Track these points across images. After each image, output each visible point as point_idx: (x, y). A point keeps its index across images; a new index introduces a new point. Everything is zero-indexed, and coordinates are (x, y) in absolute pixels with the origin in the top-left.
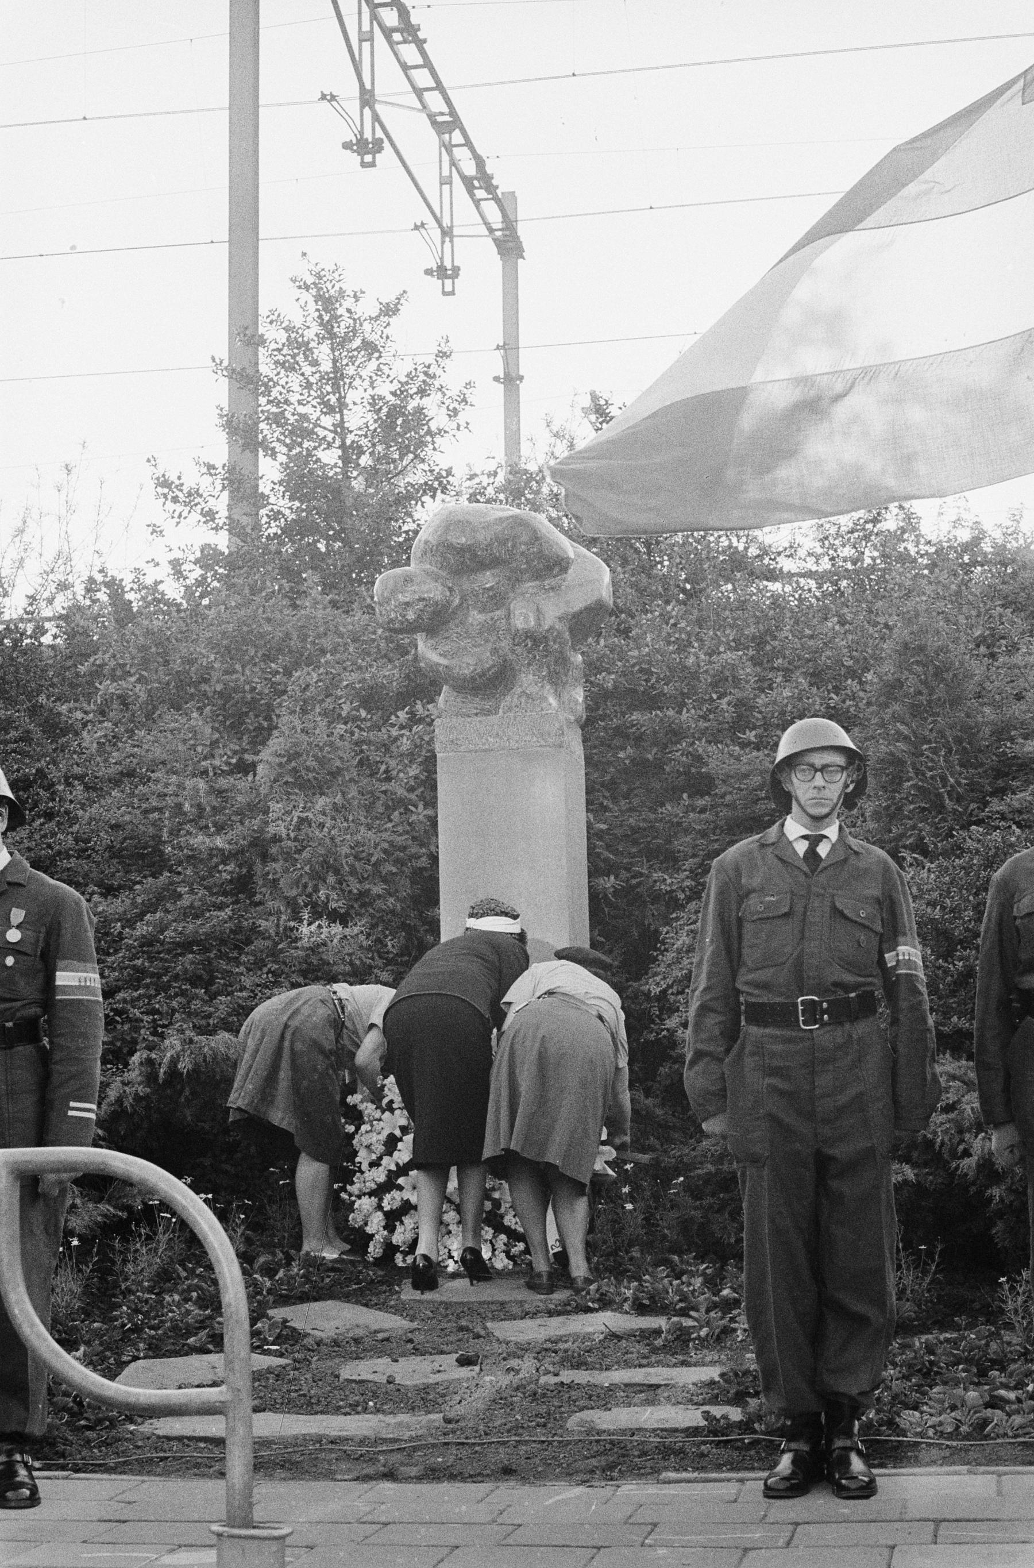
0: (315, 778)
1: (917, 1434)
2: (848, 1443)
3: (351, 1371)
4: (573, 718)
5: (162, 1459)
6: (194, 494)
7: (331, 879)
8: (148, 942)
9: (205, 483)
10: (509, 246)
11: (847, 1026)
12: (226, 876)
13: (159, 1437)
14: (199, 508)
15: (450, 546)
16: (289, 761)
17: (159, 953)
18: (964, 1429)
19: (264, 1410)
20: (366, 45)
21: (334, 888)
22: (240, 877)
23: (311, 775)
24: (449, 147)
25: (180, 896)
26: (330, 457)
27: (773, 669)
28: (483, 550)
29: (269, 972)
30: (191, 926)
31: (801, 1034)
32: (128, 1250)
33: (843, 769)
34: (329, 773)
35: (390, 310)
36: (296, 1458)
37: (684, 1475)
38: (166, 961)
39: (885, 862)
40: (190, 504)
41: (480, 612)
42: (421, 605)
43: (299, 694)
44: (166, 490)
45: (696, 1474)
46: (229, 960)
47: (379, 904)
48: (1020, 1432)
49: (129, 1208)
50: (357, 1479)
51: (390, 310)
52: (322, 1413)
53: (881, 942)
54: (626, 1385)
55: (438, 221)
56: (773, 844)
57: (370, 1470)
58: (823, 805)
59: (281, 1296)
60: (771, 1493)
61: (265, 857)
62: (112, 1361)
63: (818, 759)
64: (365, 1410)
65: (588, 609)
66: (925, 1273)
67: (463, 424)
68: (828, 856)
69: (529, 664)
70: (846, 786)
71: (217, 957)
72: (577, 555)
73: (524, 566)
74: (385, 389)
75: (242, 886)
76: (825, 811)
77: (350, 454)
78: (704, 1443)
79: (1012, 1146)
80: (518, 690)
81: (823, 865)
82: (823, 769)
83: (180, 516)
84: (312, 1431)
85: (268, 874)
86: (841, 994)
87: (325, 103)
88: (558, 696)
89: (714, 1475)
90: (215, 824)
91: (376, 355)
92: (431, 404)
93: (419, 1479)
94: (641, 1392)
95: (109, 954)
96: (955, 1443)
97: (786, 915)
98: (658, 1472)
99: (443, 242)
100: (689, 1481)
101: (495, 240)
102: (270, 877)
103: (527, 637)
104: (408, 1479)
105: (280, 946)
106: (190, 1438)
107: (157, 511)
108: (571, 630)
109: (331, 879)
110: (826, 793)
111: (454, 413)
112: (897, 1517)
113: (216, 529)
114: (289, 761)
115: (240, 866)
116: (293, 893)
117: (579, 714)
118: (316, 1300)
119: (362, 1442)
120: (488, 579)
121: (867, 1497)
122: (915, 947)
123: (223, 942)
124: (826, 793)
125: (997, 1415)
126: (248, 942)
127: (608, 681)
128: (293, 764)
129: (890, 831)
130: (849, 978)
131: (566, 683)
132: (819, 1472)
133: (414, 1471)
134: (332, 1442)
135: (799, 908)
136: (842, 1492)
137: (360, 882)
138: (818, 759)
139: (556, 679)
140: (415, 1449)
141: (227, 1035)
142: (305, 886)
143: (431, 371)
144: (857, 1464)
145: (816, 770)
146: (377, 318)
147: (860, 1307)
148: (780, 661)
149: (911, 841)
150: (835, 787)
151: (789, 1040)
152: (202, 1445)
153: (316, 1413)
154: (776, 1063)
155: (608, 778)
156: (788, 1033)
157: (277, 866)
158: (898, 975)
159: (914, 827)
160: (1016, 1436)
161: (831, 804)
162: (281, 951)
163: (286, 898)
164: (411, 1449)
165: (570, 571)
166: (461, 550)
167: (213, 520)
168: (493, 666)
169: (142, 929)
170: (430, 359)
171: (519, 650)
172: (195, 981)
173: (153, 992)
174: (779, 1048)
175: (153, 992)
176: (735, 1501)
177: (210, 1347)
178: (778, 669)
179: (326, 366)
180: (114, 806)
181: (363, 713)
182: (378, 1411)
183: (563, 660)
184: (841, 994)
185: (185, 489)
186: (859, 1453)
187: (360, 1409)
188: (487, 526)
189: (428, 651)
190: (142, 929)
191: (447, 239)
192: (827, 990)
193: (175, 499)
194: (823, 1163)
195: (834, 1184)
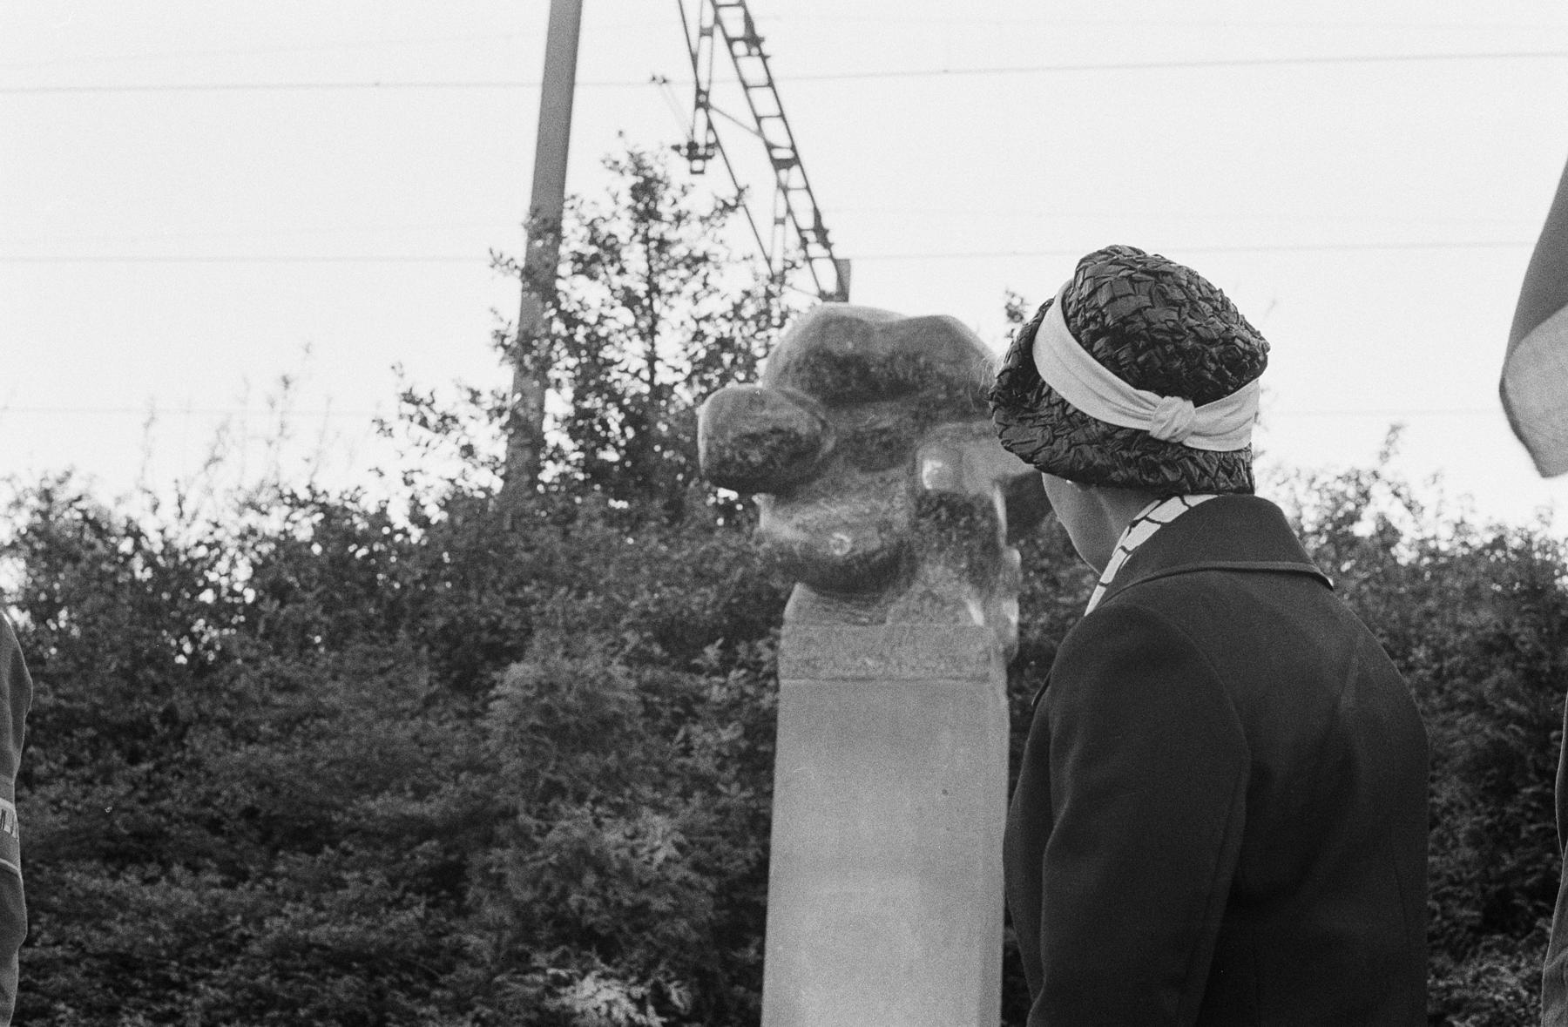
6: (446, 422)
7: (590, 879)
8: (283, 949)
9: (463, 410)
12: (421, 861)
15: (827, 356)
16: (540, 695)
17: (297, 969)
20: (706, 40)
21: (592, 894)
24: (785, 189)
25: (343, 885)
28: (879, 365)
41: (863, 470)
42: (774, 441)
46: (415, 994)
47: (663, 927)
61: (488, 841)
69: (940, 549)
71: (392, 985)
73: (942, 397)
75: (446, 883)
80: (918, 588)
85: (490, 865)
87: (654, 86)
90: (415, 788)
95: (217, 966)
102: (493, 870)
103: (941, 503)
105: (498, 979)
109: (590, 879)
114: (540, 695)
116: (527, 896)
120: (883, 417)
123: (407, 966)
128: (545, 700)
137: (635, 891)
139: (982, 575)
142: (548, 888)
149: (1530, 881)
157: (508, 855)
159: (1538, 859)
162: (499, 986)
163: (516, 904)
166: (843, 364)
171: (926, 523)
181: (657, 650)
185: (438, 408)
193: (424, 422)
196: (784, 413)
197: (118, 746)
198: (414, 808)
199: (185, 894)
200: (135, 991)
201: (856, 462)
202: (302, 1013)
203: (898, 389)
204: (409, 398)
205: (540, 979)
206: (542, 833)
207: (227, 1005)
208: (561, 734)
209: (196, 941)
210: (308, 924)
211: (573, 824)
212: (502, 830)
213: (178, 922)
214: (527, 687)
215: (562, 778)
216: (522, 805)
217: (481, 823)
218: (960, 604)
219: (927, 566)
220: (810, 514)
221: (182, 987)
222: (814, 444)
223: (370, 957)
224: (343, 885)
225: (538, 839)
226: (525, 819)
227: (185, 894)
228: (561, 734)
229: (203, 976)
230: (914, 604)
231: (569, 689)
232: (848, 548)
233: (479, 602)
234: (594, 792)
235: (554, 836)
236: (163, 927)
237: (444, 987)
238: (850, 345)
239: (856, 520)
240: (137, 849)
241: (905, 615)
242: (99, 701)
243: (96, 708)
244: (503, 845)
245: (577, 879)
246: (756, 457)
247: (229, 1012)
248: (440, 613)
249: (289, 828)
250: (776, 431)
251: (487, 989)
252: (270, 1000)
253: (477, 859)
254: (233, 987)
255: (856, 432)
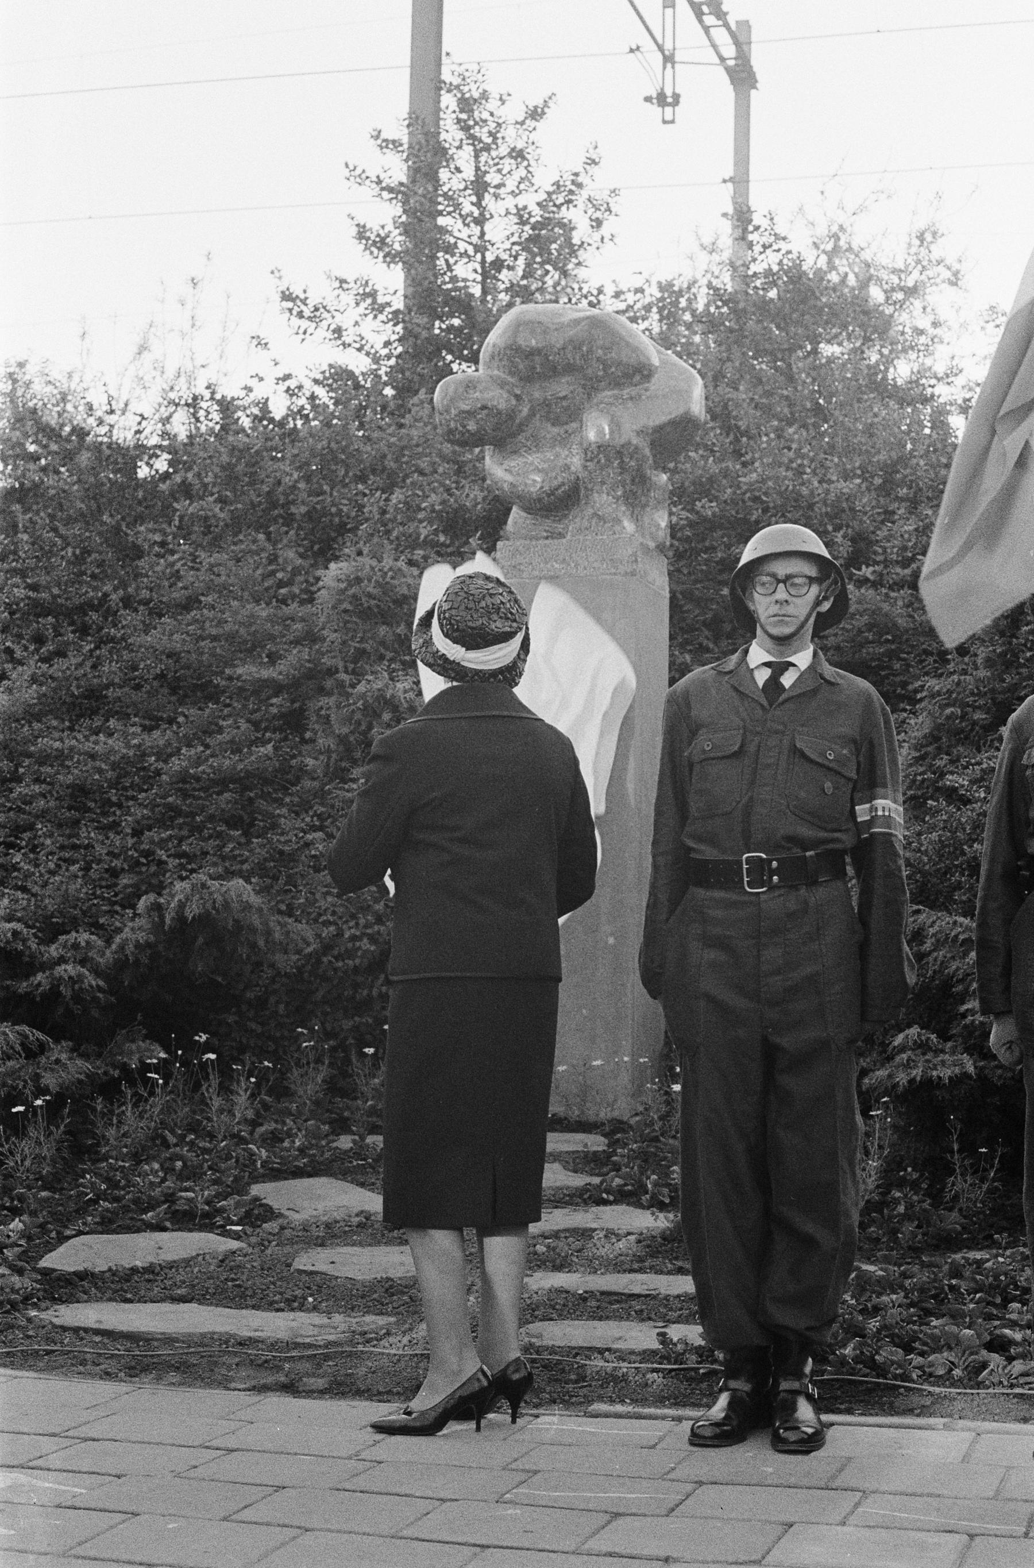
0: (378, 606)
1: (896, 1377)
2: (796, 1385)
3: (314, 1260)
4: (652, 545)
5: (48, 1353)
8: (184, 777)
10: (742, 76)
11: (803, 891)
12: (274, 710)
13: (55, 1326)
14: (325, 324)
18: (957, 1372)
19: (190, 1302)
22: (292, 713)
23: (373, 602)
26: (466, 271)
27: (896, 498)
29: (315, 814)
30: (227, 762)
31: (746, 898)
32: (111, 1112)
33: (811, 580)
34: (395, 602)
35: (536, 114)
36: (193, 1360)
37: (619, 1408)
38: (200, 798)
39: (869, 698)
40: (315, 318)
41: (553, 425)
43: (377, 517)
44: (290, 305)
45: (630, 1409)
48: (1022, 1380)
49: (124, 1068)
50: (253, 1389)
51: (536, 114)
52: (254, 1307)
53: (854, 790)
54: (603, 1293)
55: (661, 48)
56: (731, 672)
57: (270, 1380)
58: (787, 623)
59: (272, 1169)
60: (697, 1439)
61: (322, 691)
62: (53, 1234)
63: (782, 569)
64: (301, 1308)
65: (673, 423)
66: (983, 1180)
67: (607, 237)
68: (793, 685)
70: (818, 603)
72: (664, 363)
73: (601, 373)
74: (530, 200)
75: (293, 723)
76: (788, 630)
77: (490, 271)
78: (654, 1370)
79: (1011, 1042)
81: (784, 696)
82: (787, 579)
83: (305, 333)
84: (219, 1329)
86: (797, 852)
88: (636, 520)
89: (652, 1411)
91: (525, 163)
92: (577, 216)
93: (322, 1393)
94: (618, 1302)
96: (937, 1390)
97: (735, 755)
98: (590, 1402)
99: (664, 68)
100: (618, 1416)
101: (728, 69)
102: (323, 712)
104: (309, 1394)
106: (86, 1330)
107: (279, 326)
108: (653, 444)
110: (790, 610)
111: (598, 223)
112: (822, 1484)
113: (345, 345)
114: (350, 585)
115: (293, 702)
116: (345, 730)
117: (660, 540)
118: (310, 1176)
119: (273, 1345)
120: (563, 387)
121: (807, 1452)
122: (895, 802)
123: (266, 782)
124: (790, 610)
125: (996, 1359)
126: (298, 780)
127: (708, 508)
129: (1003, 681)
130: (805, 831)
131: (645, 505)
132: (758, 1418)
133: (320, 1383)
134: (240, 1344)
135: (752, 748)
136: (780, 1445)
138: (782, 569)
140: (327, 1357)
141: (241, 881)
142: (359, 723)
143: (580, 179)
144: (805, 1411)
145: (779, 581)
146: (522, 123)
147: (809, 1228)
148: (905, 490)
150: (804, 602)
151: (734, 904)
152: (98, 1339)
153: (247, 1307)
154: (717, 931)
155: (709, 616)
156: (733, 896)
157: (332, 701)
158: (872, 835)
160: (1012, 1386)
161: (797, 623)
162: (330, 792)
164: (319, 1356)
165: (653, 380)
166: (530, 354)
167: (339, 337)
168: (563, 484)
169: (176, 764)
170: (579, 169)
172: (233, 822)
173: (185, 832)
174: (719, 913)
175: (185, 832)
176: (653, 1447)
177: (168, 1224)
178: (902, 500)
179: (469, 173)
180: (166, 635)
182: (315, 1309)
183: (641, 480)
184: (797, 852)
186: (809, 1398)
187: (296, 1304)
188: (560, 328)
189: (499, 470)
190: (176, 764)
191: (669, 65)
192: (778, 847)
193: (300, 315)
194: (770, 1053)
195: (787, 1081)
196: (488, 395)
197: (72, 623)
198: (266, 673)
199: (117, 741)
200: (89, 810)
201: (548, 420)
202: (198, 819)
203: (570, 369)
204: (287, 296)
205: (355, 786)
206: (353, 686)
207: (149, 818)
208: (365, 614)
209: (127, 774)
210: (199, 761)
211: (374, 683)
212: (329, 683)
213: (114, 763)
214: (339, 580)
215: (367, 646)
216: (341, 665)
217: (314, 679)
218: (618, 521)
219: (596, 495)
220: (515, 462)
221: (120, 806)
222: (511, 415)
223: (241, 779)
224: (220, 730)
225: (350, 690)
226: (343, 676)
227: (117, 741)
228: (365, 614)
229: (133, 798)
230: (586, 524)
231: (369, 581)
232: (538, 486)
233: (331, 495)
234: (389, 655)
235: (361, 688)
236: (103, 766)
237: (291, 795)
238: (534, 342)
239: (546, 466)
240: (86, 706)
241: (580, 530)
242: (56, 591)
243: (55, 597)
244: (329, 694)
245: (377, 715)
246: (472, 426)
247: (151, 822)
248: (303, 503)
249: (187, 684)
250: (484, 407)
251: (321, 795)
252: (177, 812)
253: (312, 705)
254: (153, 806)
255: (545, 399)
